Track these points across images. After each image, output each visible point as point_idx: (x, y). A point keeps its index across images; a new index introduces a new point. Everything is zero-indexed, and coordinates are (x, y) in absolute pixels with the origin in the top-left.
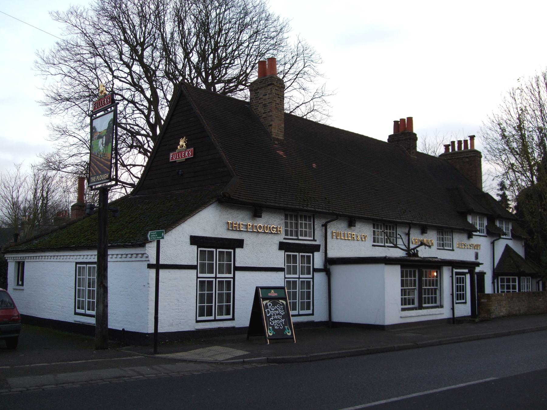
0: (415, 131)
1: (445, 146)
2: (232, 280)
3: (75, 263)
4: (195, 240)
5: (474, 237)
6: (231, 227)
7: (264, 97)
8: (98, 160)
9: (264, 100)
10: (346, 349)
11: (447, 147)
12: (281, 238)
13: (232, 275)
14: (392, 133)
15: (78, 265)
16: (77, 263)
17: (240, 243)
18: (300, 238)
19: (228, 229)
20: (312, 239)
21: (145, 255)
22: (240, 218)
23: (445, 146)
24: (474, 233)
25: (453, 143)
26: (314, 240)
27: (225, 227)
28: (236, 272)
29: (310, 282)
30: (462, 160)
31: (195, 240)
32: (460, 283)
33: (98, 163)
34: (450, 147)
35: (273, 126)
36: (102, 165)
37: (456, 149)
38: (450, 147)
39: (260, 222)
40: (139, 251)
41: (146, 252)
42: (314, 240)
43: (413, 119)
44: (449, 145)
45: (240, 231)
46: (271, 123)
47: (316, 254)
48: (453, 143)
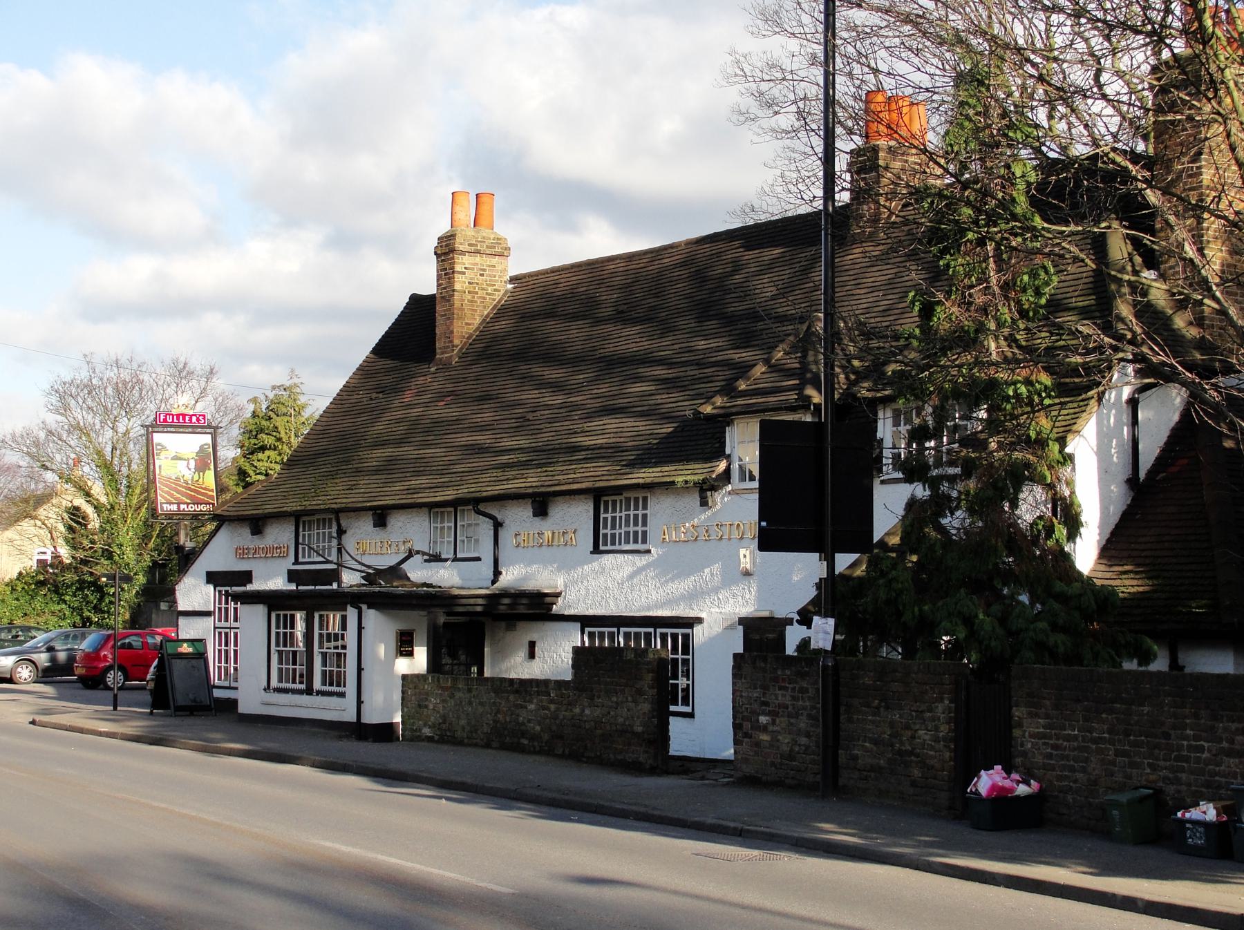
6: (241, 553)
31: (213, 578)
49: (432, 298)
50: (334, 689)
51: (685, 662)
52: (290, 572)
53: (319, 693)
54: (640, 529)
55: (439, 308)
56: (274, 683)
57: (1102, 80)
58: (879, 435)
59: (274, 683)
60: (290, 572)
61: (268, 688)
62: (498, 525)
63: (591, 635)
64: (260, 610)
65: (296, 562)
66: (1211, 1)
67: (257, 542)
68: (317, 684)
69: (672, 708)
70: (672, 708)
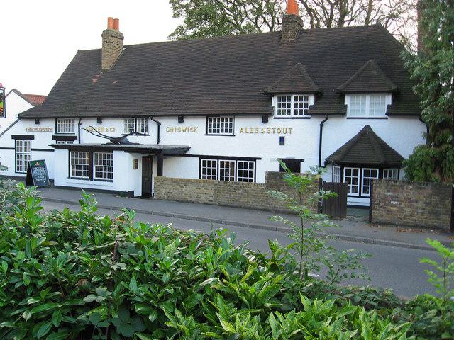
4: (13, 137)
12: (53, 133)
17: (32, 138)
22: (32, 124)
49: (101, 50)
50: (79, 177)
51: (251, 172)
52: (53, 136)
53: (95, 180)
54: (145, 128)
55: (103, 54)
56: (71, 176)
57: (310, 17)
58: (273, 105)
59: (71, 176)
60: (53, 136)
61: (69, 177)
62: (159, 125)
63: (348, 173)
64: (66, 151)
65: (56, 133)
66: (441, 1)
67: (36, 126)
68: (94, 177)
69: (348, 194)
70: (348, 194)
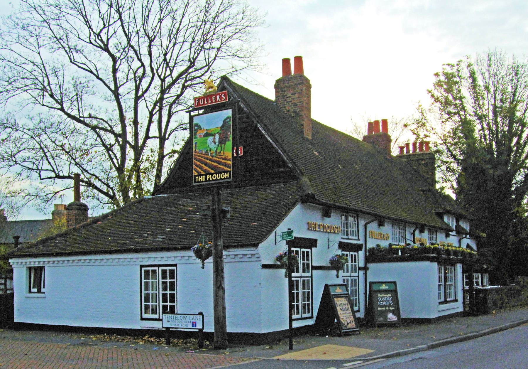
0: (389, 133)
1: (399, 147)
2: (310, 279)
3: (139, 267)
5: (450, 236)
7: (293, 96)
8: (210, 160)
9: (293, 99)
10: (442, 339)
11: (401, 148)
13: (309, 275)
14: (366, 134)
15: (143, 269)
16: (142, 266)
18: (350, 237)
19: (308, 229)
20: (357, 238)
21: (257, 256)
23: (399, 147)
24: (451, 233)
25: (407, 145)
26: (359, 239)
27: (306, 226)
28: (314, 271)
29: (355, 280)
30: (421, 161)
32: (152, 294)
33: (208, 161)
34: (405, 149)
35: (305, 125)
36: (216, 164)
37: (411, 152)
38: (405, 149)
39: (328, 222)
40: (248, 251)
41: (259, 252)
42: (359, 239)
43: (388, 121)
44: (404, 147)
45: (315, 230)
46: (302, 123)
47: (360, 252)
48: (407, 145)
